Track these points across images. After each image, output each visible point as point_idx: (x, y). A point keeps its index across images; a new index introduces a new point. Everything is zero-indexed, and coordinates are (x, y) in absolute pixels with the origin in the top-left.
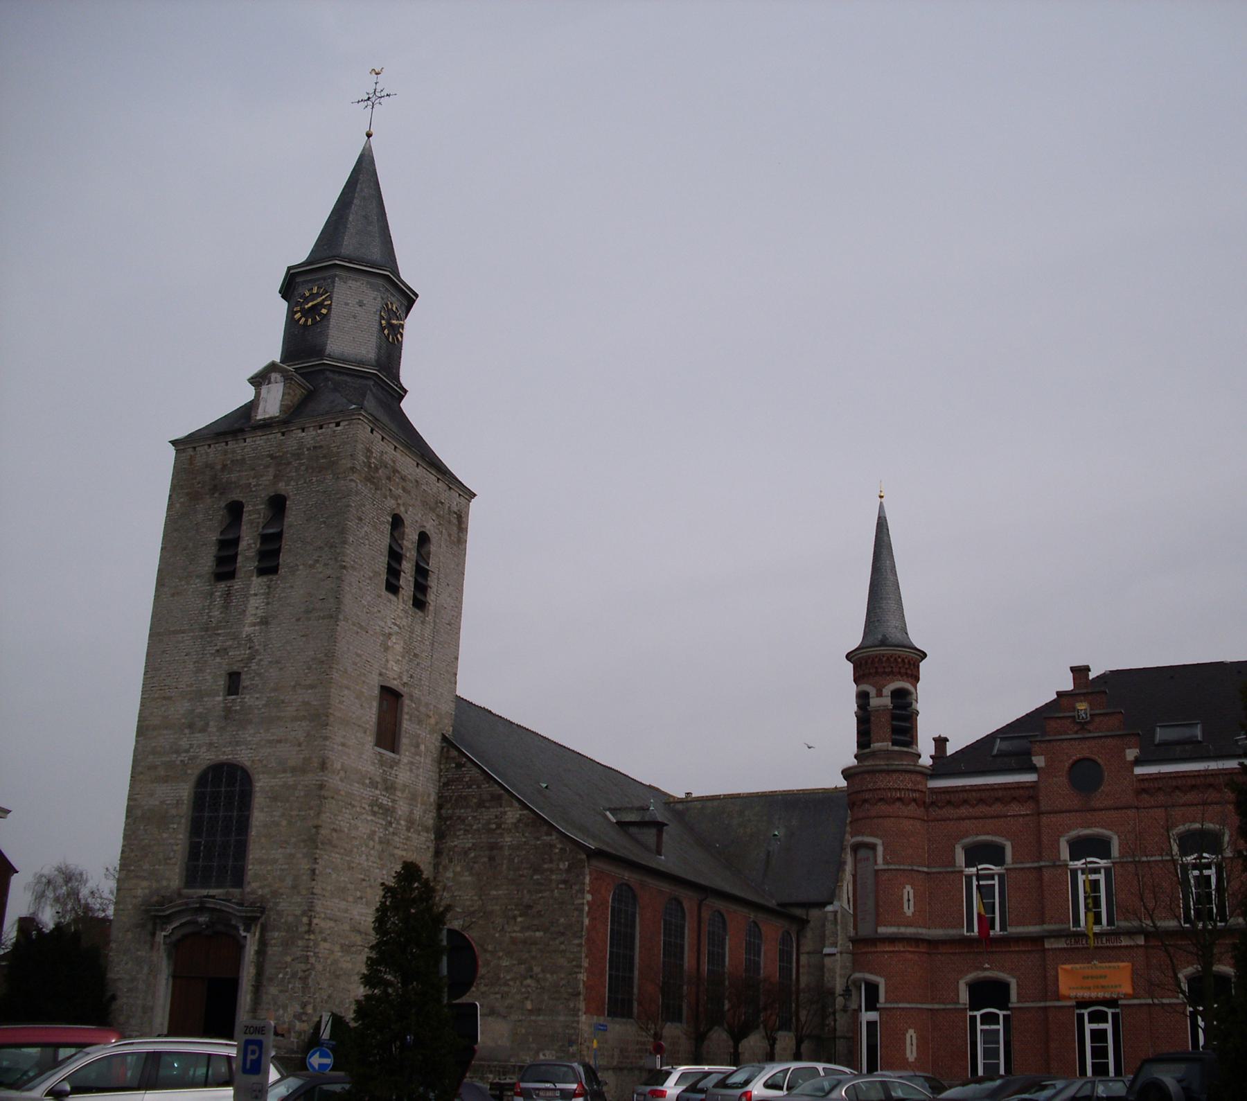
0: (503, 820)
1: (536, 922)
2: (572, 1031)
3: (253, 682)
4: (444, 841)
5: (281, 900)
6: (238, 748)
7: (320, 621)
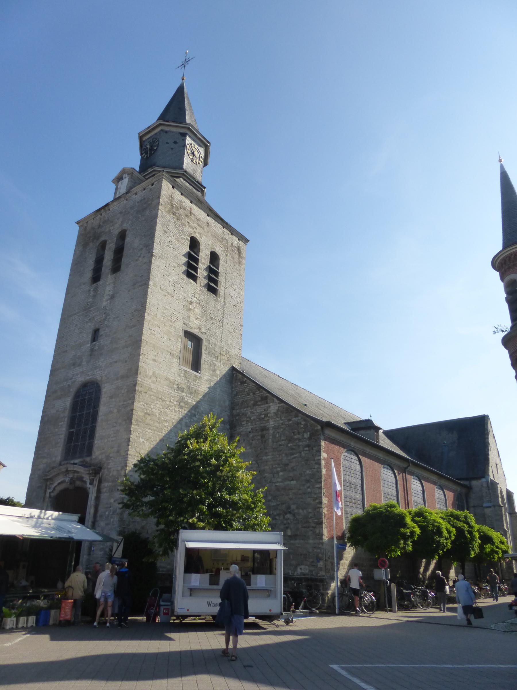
0: (268, 411)
1: (291, 474)
2: (319, 551)
3: (105, 332)
4: (235, 429)
5: (111, 461)
6: (95, 371)
7: (140, 288)
